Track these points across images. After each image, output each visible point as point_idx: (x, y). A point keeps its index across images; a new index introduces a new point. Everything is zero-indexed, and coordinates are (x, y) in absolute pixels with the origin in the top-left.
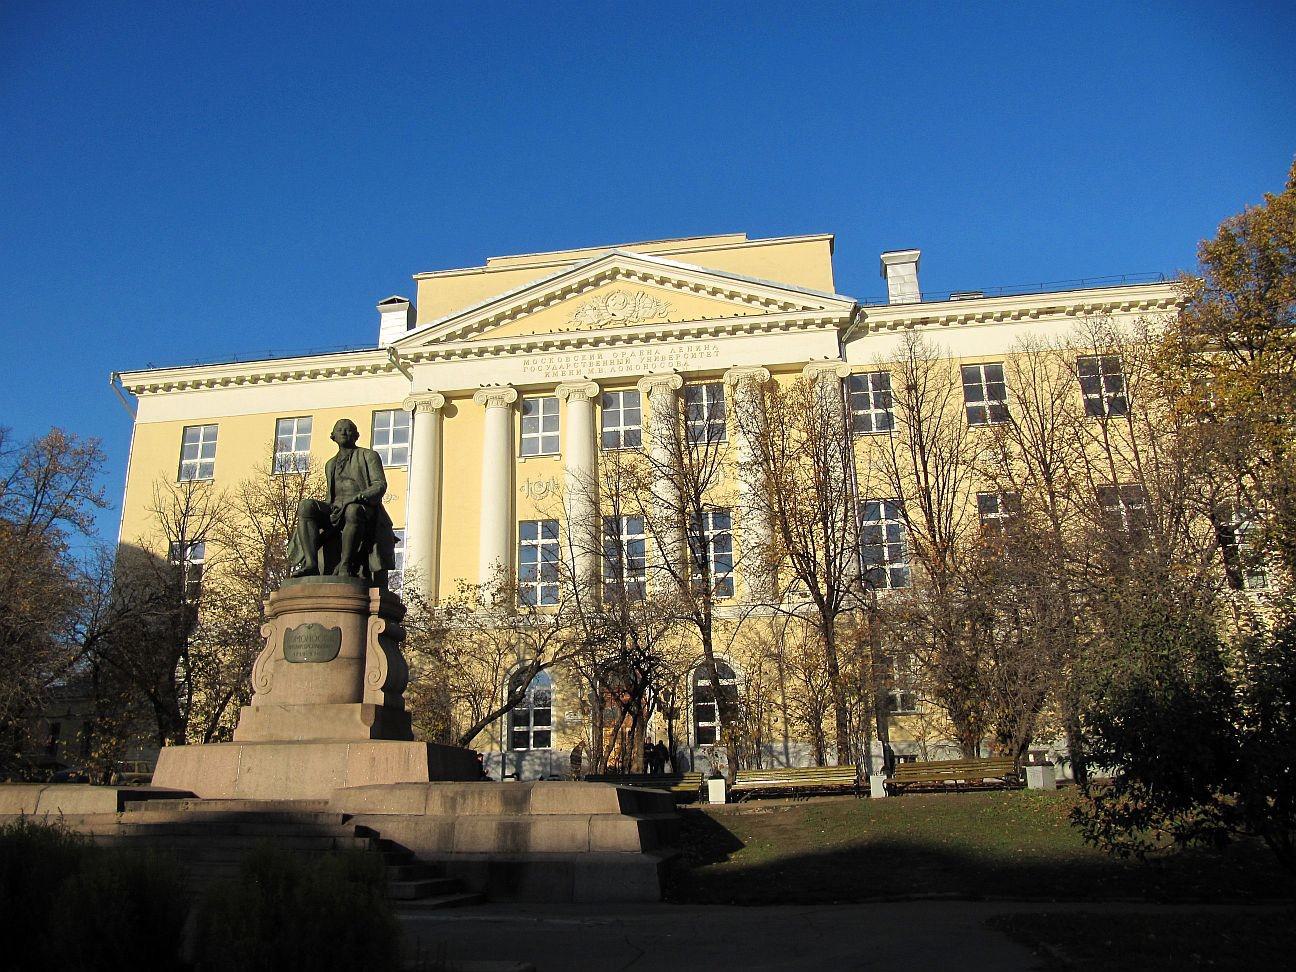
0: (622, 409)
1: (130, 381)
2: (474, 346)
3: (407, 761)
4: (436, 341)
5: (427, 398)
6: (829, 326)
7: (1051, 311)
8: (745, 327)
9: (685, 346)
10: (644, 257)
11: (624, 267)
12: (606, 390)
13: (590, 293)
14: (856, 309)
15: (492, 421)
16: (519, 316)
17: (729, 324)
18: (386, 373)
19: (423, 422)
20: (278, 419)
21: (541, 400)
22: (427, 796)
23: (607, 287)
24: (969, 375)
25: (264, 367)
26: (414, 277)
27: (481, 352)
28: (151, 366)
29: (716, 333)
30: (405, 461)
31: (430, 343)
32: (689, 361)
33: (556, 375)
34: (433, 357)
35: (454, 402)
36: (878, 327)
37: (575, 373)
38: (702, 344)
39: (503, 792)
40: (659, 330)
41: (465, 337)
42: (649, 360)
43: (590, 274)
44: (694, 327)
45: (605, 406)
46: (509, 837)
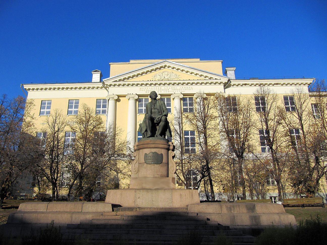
0: (144, 103)
1: (26, 87)
2: (127, 83)
3: (192, 196)
4: (116, 81)
5: (113, 96)
6: (222, 84)
7: (277, 84)
8: (154, 84)
9: (184, 87)
10: (174, 63)
11: (168, 64)
12: (139, 97)
15: (131, 103)
16: (139, 76)
17: (196, 82)
18: (101, 89)
19: (111, 104)
20: (69, 100)
21: (144, 99)
22: (221, 207)
23: (163, 70)
24: (285, 98)
25: (74, 85)
26: (110, 63)
27: (128, 85)
28: (32, 83)
29: (192, 84)
30: (106, 113)
31: (114, 81)
32: (185, 91)
34: (115, 85)
35: (120, 98)
36: (234, 85)
38: (188, 87)
39: (246, 206)
40: (177, 82)
41: (123, 81)
42: (174, 90)
43: (159, 66)
44: (186, 82)
45: (139, 102)
46: (253, 220)
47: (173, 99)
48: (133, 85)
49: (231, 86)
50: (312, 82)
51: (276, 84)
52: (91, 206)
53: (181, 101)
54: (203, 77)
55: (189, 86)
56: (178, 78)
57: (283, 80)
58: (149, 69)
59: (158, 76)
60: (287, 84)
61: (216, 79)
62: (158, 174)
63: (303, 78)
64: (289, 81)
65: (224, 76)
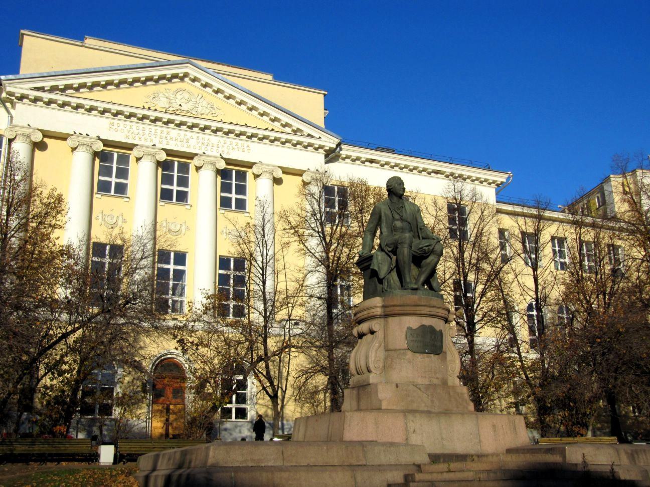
2: (74, 101)
3: (515, 428)
4: (41, 89)
5: (27, 131)
6: (321, 151)
7: (437, 172)
8: (99, 109)
9: (228, 141)
11: (193, 72)
13: (163, 86)
14: (339, 145)
15: (82, 159)
17: (261, 133)
23: (176, 85)
26: (22, 31)
27: (77, 107)
31: (36, 89)
32: (230, 151)
33: (134, 138)
34: (35, 100)
36: (348, 157)
37: (149, 140)
38: (240, 142)
41: (61, 91)
43: (169, 72)
44: (238, 129)
47: (138, 159)
48: (91, 109)
49: (338, 160)
50: (505, 181)
51: (435, 173)
52: (384, 451)
53: (94, 160)
54: (279, 124)
55: (243, 142)
56: (214, 115)
57: (450, 165)
58: (143, 75)
59: (164, 99)
60: (404, 168)
61: (309, 135)
62: (437, 378)
63: (488, 168)
64: (351, 150)
65: (326, 130)
